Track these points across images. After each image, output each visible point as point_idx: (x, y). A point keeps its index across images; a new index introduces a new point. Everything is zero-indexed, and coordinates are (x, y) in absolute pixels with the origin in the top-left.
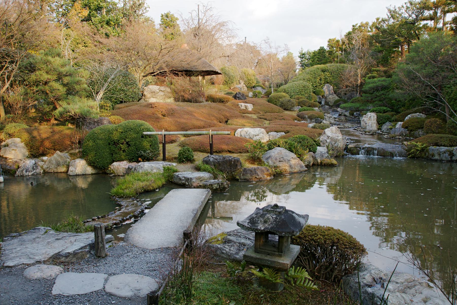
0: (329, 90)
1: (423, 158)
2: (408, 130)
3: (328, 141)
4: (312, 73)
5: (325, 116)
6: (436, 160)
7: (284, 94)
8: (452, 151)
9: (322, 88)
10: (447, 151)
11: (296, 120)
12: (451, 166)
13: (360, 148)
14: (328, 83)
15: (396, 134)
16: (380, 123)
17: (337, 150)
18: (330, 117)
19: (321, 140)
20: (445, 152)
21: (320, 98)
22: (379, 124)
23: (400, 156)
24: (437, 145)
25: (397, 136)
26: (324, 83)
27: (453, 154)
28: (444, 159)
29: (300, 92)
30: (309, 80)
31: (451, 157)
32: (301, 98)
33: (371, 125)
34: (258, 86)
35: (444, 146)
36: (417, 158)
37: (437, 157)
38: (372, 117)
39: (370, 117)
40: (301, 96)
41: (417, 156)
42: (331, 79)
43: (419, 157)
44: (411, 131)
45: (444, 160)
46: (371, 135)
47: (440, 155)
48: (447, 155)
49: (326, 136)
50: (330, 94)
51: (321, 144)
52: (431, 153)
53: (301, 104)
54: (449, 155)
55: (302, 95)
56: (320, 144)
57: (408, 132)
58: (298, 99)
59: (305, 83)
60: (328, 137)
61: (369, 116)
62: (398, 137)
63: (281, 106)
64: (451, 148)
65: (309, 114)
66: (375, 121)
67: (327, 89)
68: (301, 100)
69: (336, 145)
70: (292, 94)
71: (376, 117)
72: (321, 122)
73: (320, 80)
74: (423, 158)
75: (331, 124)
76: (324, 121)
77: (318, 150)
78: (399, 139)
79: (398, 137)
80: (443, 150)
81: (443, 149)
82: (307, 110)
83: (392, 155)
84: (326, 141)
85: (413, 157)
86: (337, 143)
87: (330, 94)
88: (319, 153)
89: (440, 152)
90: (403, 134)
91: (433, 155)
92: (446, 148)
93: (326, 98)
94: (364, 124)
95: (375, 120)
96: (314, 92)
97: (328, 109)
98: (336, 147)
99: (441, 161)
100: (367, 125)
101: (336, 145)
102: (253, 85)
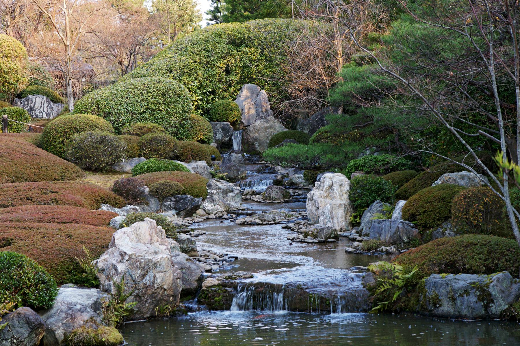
0: (258, 106)
1: (413, 312)
2: (416, 226)
3: (121, 268)
4: (197, 49)
5: (210, 186)
6: (446, 318)
7: (92, 117)
8: (487, 286)
9: (234, 96)
10: (474, 286)
11: (105, 202)
12: (488, 332)
13: (235, 288)
14: (252, 80)
15: (383, 238)
16: (358, 204)
17: (152, 296)
18: (225, 192)
19: (100, 265)
20: (466, 292)
21: (224, 129)
22: (355, 208)
23: (346, 309)
24: (453, 268)
25: (385, 244)
26: (242, 82)
27: (490, 295)
28: (465, 312)
29: (151, 112)
30: (186, 72)
31: (486, 307)
32: (149, 131)
33: (331, 212)
34: (33, 92)
35: (468, 271)
36: (396, 312)
37: (446, 307)
38: (336, 187)
39: (331, 186)
40: (150, 125)
41: (397, 306)
42: (260, 68)
43: (401, 311)
44: (426, 227)
45: (466, 316)
46: (320, 243)
47: (453, 299)
48: (473, 299)
49: (116, 254)
50: (258, 116)
51: (102, 278)
52: (430, 294)
53: (148, 149)
54: (480, 298)
55: (157, 121)
56: (96, 278)
57: (415, 231)
58: (141, 132)
59: (169, 82)
60: (122, 254)
61: (328, 183)
62: (384, 248)
63: (77, 160)
64: (484, 278)
65: (156, 184)
66: (345, 200)
67: (249, 102)
68: (150, 136)
69: (147, 280)
70: (123, 118)
71: (347, 188)
72: (197, 207)
73: (228, 71)
74: (413, 312)
75: (228, 212)
76: (207, 205)
77: (59, 298)
78: (388, 253)
79: (384, 248)
80: (462, 283)
81: (464, 280)
82: (158, 170)
83: (325, 304)
84: (116, 269)
85: (386, 312)
86: (152, 273)
87: (258, 116)
88: (64, 308)
89: (454, 291)
90: (401, 238)
91: (437, 302)
92: (473, 278)
93: (245, 129)
94: (314, 209)
95: (346, 196)
96: (206, 112)
97: (241, 165)
98: (146, 287)
99: (458, 319)
100: (320, 211)
101: (147, 280)
102: (21, 87)
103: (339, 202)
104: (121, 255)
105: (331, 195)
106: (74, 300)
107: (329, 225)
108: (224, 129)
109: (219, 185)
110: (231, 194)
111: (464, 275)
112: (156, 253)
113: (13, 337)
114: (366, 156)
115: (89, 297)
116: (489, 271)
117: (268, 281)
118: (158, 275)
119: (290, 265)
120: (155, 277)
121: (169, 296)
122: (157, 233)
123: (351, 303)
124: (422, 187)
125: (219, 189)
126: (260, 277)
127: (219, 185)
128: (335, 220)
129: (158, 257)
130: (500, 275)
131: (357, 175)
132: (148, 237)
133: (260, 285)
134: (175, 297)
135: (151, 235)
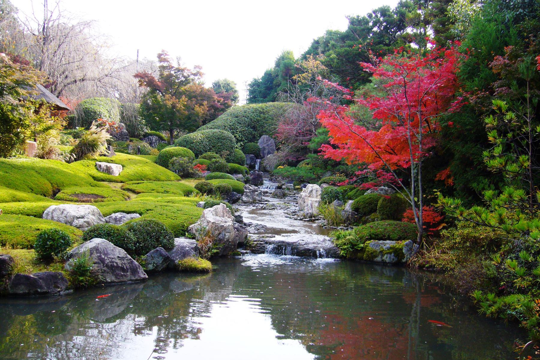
6: (378, 263)
38: (314, 192)
39: (312, 191)
49: (205, 221)
61: (310, 189)
71: (320, 192)
72: (239, 199)
81: (389, 244)
82: (103, 180)
95: (319, 197)
99: (384, 264)
103: (316, 199)
104: (208, 222)
105: (312, 195)
106: (185, 244)
107: (310, 211)
108: (251, 158)
109: (251, 188)
110: (256, 193)
111: (388, 241)
112: (226, 222)
113: (154, 263)
114: (327, 177)
115: (192, 243)
116: (400, 239)
117: (284, 240)
118: (226, 234)
119: (294, 232)
120: (225, 235)
121: (231, 245)
122: (226, 212)
123: (329, 253)
124: (360, 195)
125: (251, 189)
126: (278, 238)
127: (251, 188)
128: (313, 209)
129: (228, 224)
130: (407, 241)
131: (325, 186)
132: (222, 213)
133: (280, 242)
134: (234, 245)
135: (223, 212)
